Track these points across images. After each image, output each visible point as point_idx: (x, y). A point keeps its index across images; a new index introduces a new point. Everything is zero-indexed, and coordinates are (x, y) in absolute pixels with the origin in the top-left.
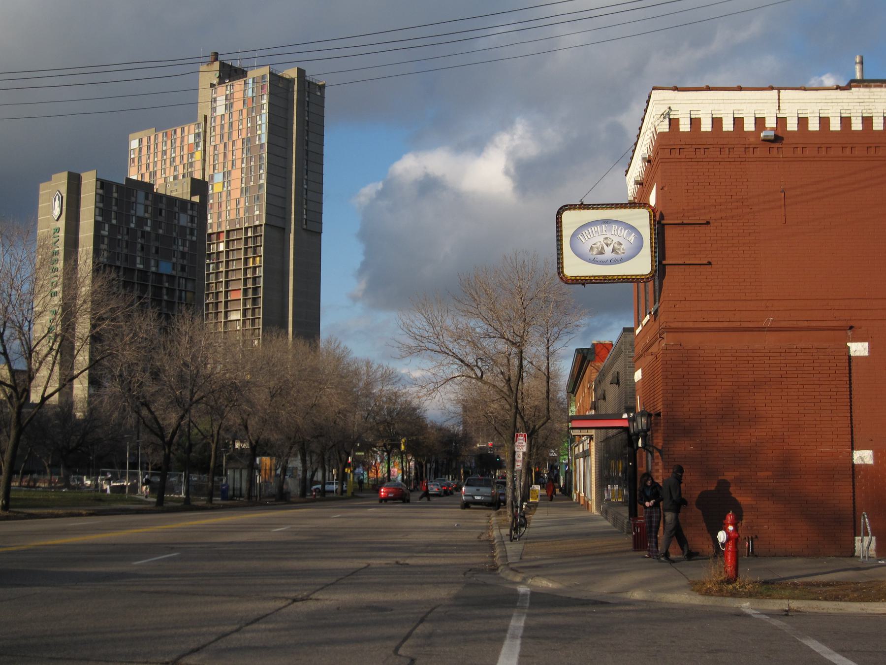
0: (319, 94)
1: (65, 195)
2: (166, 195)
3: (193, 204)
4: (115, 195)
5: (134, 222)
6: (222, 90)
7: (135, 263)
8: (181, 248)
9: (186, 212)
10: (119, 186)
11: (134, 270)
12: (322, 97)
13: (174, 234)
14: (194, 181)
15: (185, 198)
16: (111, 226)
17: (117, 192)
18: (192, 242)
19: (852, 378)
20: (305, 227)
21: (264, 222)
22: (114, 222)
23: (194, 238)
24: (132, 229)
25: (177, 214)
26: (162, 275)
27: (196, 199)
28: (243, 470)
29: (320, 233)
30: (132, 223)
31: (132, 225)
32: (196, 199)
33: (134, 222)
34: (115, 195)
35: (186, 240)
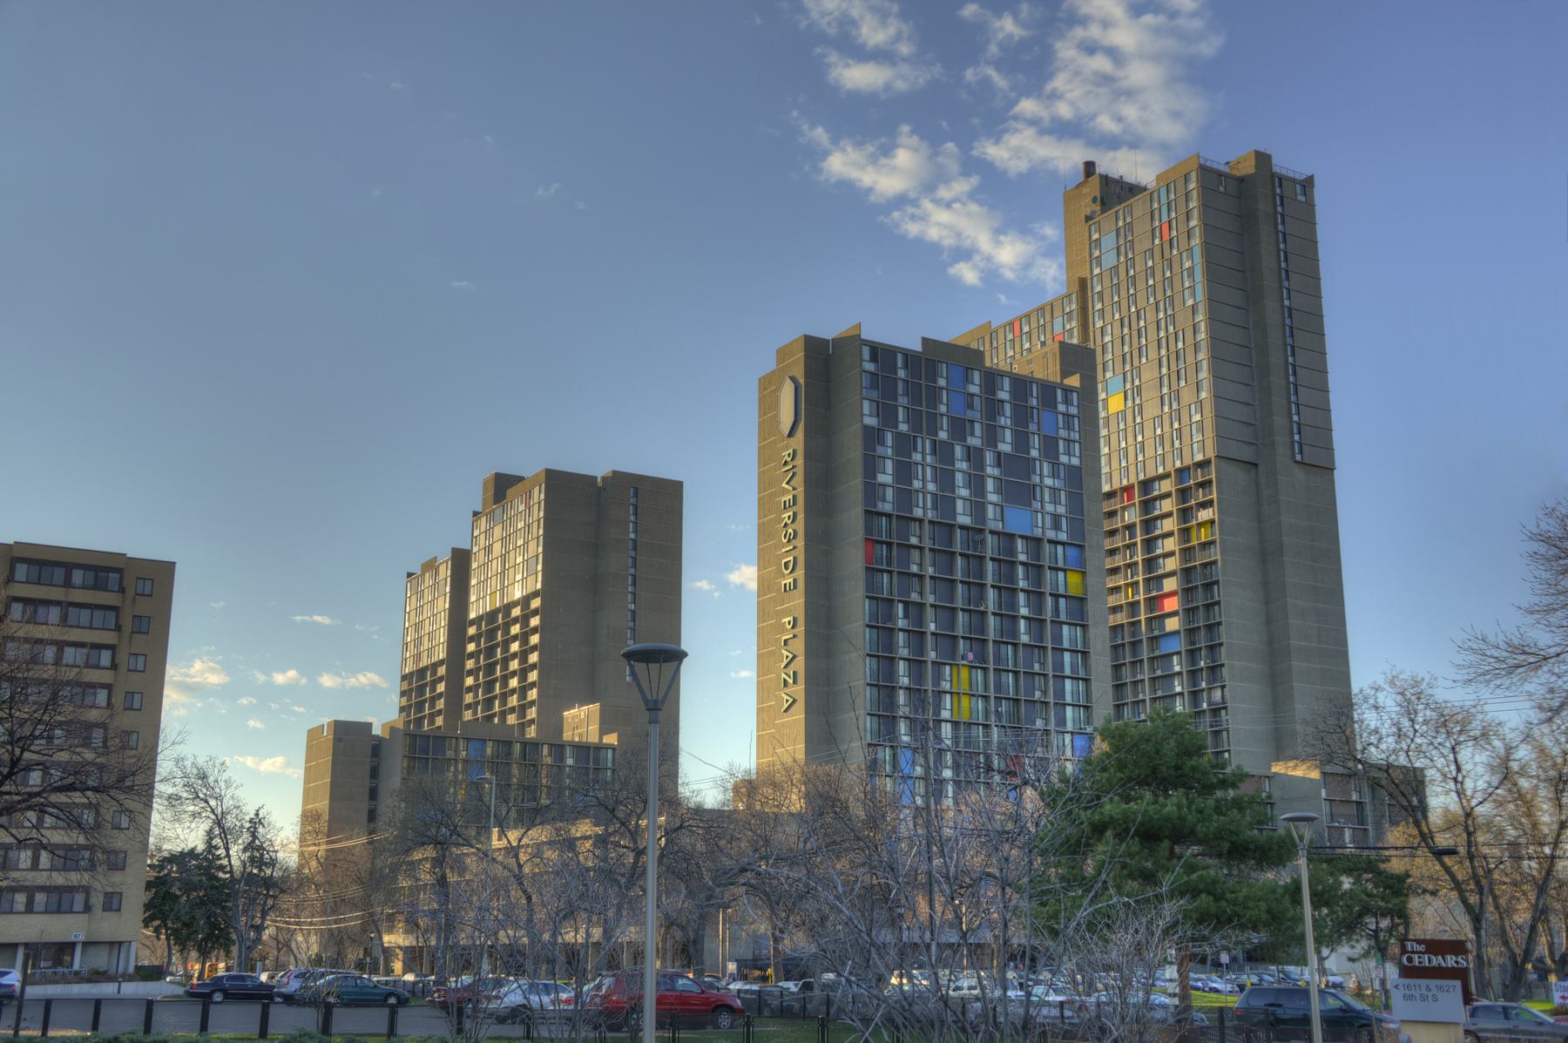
0: (1301, 198)
1: (802, 381)
2: (1011, 372)
3: (1067, 391)
4: (901, 373)
5: (945, 427)
6: (1107, 220)
7: (954, 514)
8: (1049, 508)
9: (1056, 408)
10: (908, 356)
11: (952, 526)
12: (1310, 205)
13: (1034, 453)
14: (1064, 347)
15: (1051, 379)
16: (899, 437)
17: (906, 366)
18: (1070, 467)
19: (514, 1036)
20: (1298, 457)
21: (1211, 454)
22: (903, 427)
23: (1075, 461)
24: (942, 442)
25: (1038, 462)
26: (1011, 537)
27: (1074, 381)
28: (64, 894)
29: (1330, 469)
30: (942, 429)
31: (943, 435)
32: (1074, 381)
33: (945, 427)
34: (901, 373)
35: (1065, 677)
